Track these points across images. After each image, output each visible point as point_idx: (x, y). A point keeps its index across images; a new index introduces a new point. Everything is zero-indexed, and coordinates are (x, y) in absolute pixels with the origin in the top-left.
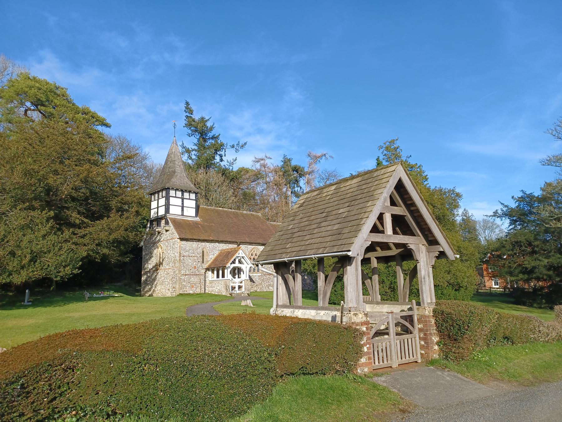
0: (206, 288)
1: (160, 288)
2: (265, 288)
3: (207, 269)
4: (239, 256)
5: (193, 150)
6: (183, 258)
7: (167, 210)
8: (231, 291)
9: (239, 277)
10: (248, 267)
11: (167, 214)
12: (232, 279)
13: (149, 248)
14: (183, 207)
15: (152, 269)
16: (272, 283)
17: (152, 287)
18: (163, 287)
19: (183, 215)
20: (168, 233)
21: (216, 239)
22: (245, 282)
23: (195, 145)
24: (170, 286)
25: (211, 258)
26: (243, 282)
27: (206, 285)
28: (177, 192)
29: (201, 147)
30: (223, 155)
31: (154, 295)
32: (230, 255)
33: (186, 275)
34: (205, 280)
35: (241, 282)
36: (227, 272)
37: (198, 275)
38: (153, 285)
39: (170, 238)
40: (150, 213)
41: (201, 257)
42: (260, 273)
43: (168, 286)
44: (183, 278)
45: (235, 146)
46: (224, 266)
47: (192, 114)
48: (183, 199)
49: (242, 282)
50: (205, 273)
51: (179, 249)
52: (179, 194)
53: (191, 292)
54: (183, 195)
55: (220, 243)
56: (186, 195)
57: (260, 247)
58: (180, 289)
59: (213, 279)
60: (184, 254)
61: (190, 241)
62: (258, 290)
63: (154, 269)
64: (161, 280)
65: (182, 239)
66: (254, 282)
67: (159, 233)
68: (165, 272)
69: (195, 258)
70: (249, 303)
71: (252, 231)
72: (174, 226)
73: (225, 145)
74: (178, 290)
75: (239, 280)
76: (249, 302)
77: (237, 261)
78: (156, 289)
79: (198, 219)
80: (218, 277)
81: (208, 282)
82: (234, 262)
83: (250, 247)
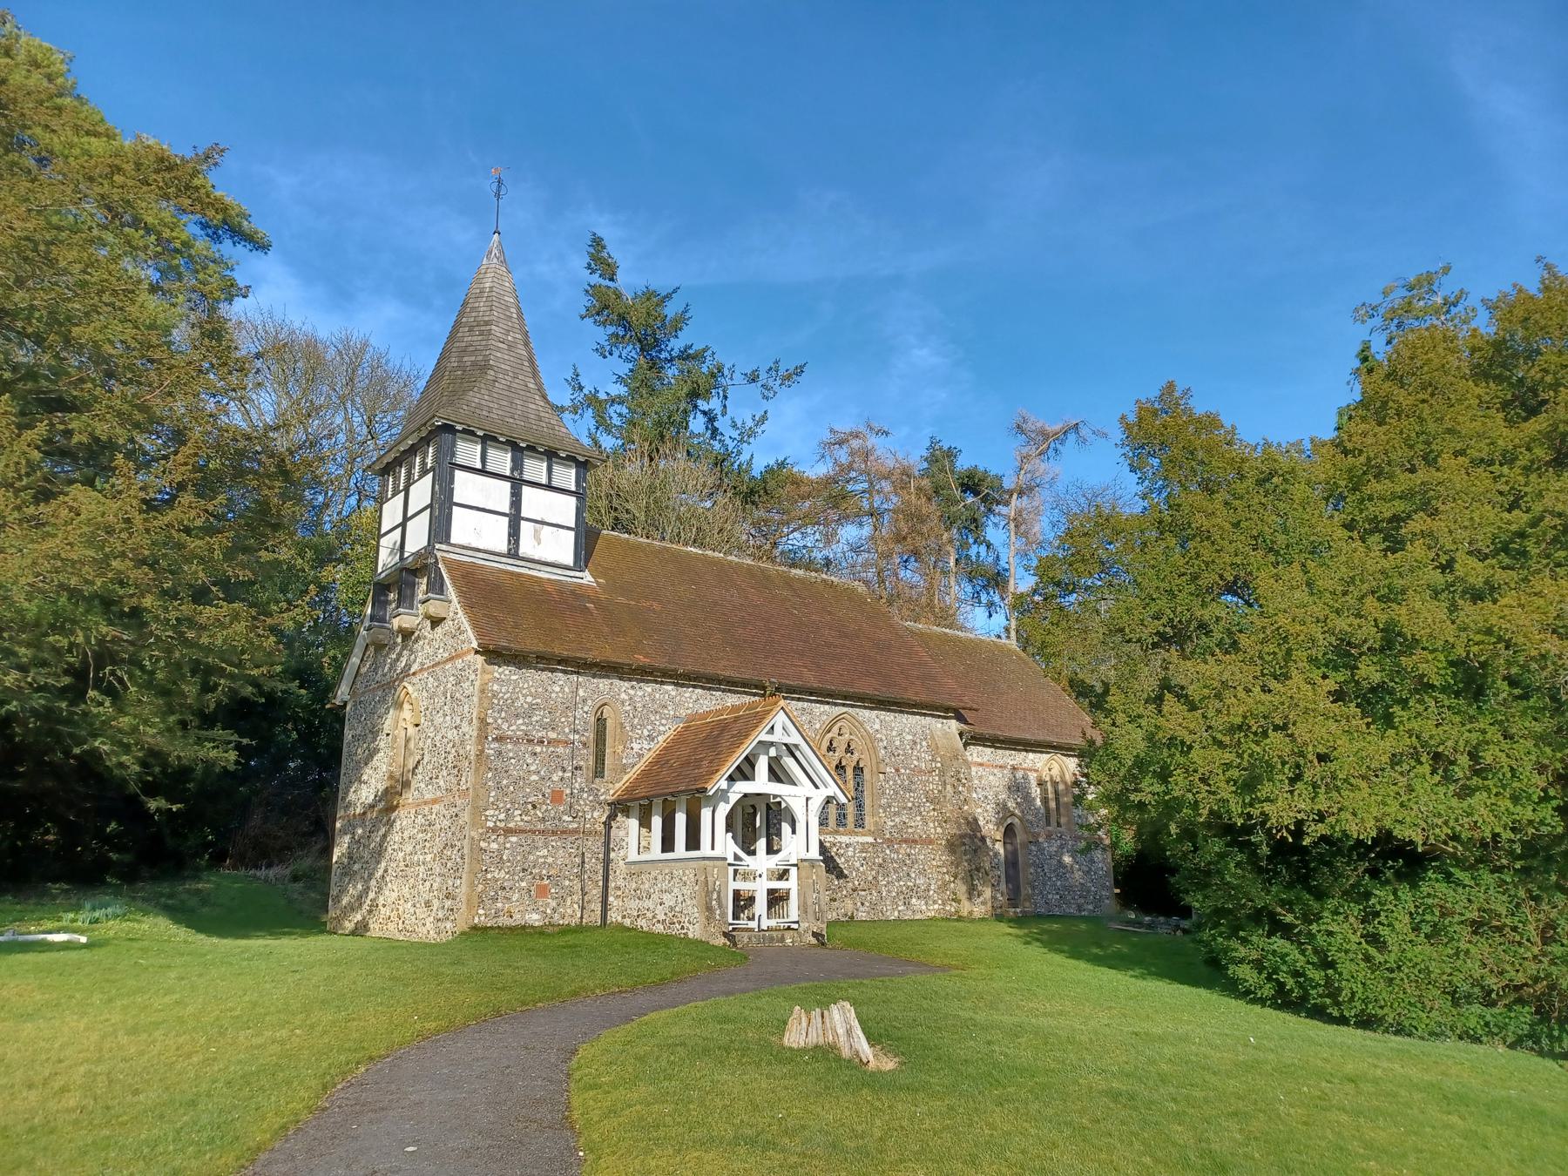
0: (611, 899)
1: (395, 895)
2: (894, 903)
3: (620, 807)
4: (772, 744)
5: (613, 401)
6: (495, 745)
7: (440, 528)
8: (730, 920)
9: (771, 850)
10: (819, 798)
11: (438, 546)
12: (737, 857)
13: (368, 710)
14: (515, 519)
15: (372, 806)
16: (920, 881)
17: (366, 890)
18: (406, 890)
19: (513, 553)
20: (439, 630)
21: (661, 663)
22: (803, 874)
23: (620, 380)
24: (435, 886)
25: (640, 756)
26: (793, 871)
27: (612, 885)
28: (492, 453)
29: (643, 383)
30: (718, 411)
31: (375, 929)
32: (727, 735)
33: (508, 832)
34: (607, 862)
35: (783, 875)
36: (714, 820)
37: (575, 831)
38: (371, 876)
39: (446, 655)
40: (377, 558)
41: (592, 745)
42: (871, 833)
43: (428, 884)
44: (494, 846)
45: (763, 376)
46: (698, 791)
47: (612, 279)
48: (517, 483)
49: (786, 872)
50: (608, 826)
51: (481, 704)
52: (501, 460)
53: (534, 919)
54: (517, 465)
55: (683, 686)
56: (535, 469)
57: (867, 713)
58: (476, 900)
59: (644, 857)
60: (505, 726)
61: (535, 668)
62: (862, 915)
63: (381, 805)
64: (401, 855)
65: (493, 655)
66: (841, 875)
67: (407, 634)
68: (420, 820)
69: (560, 750)
70: (841, 1031)
71: (828, 645)
72: (462, 594)
73: (726, 372)
74: (464, 907)
75: (773, 862)
76: (846, 1021)
77: (762, 766)
78: (381, 901)
79: (587, 578)
80: (668, 844)
81: (619, 868)
82: (745, 771)
83: (824, 712)
